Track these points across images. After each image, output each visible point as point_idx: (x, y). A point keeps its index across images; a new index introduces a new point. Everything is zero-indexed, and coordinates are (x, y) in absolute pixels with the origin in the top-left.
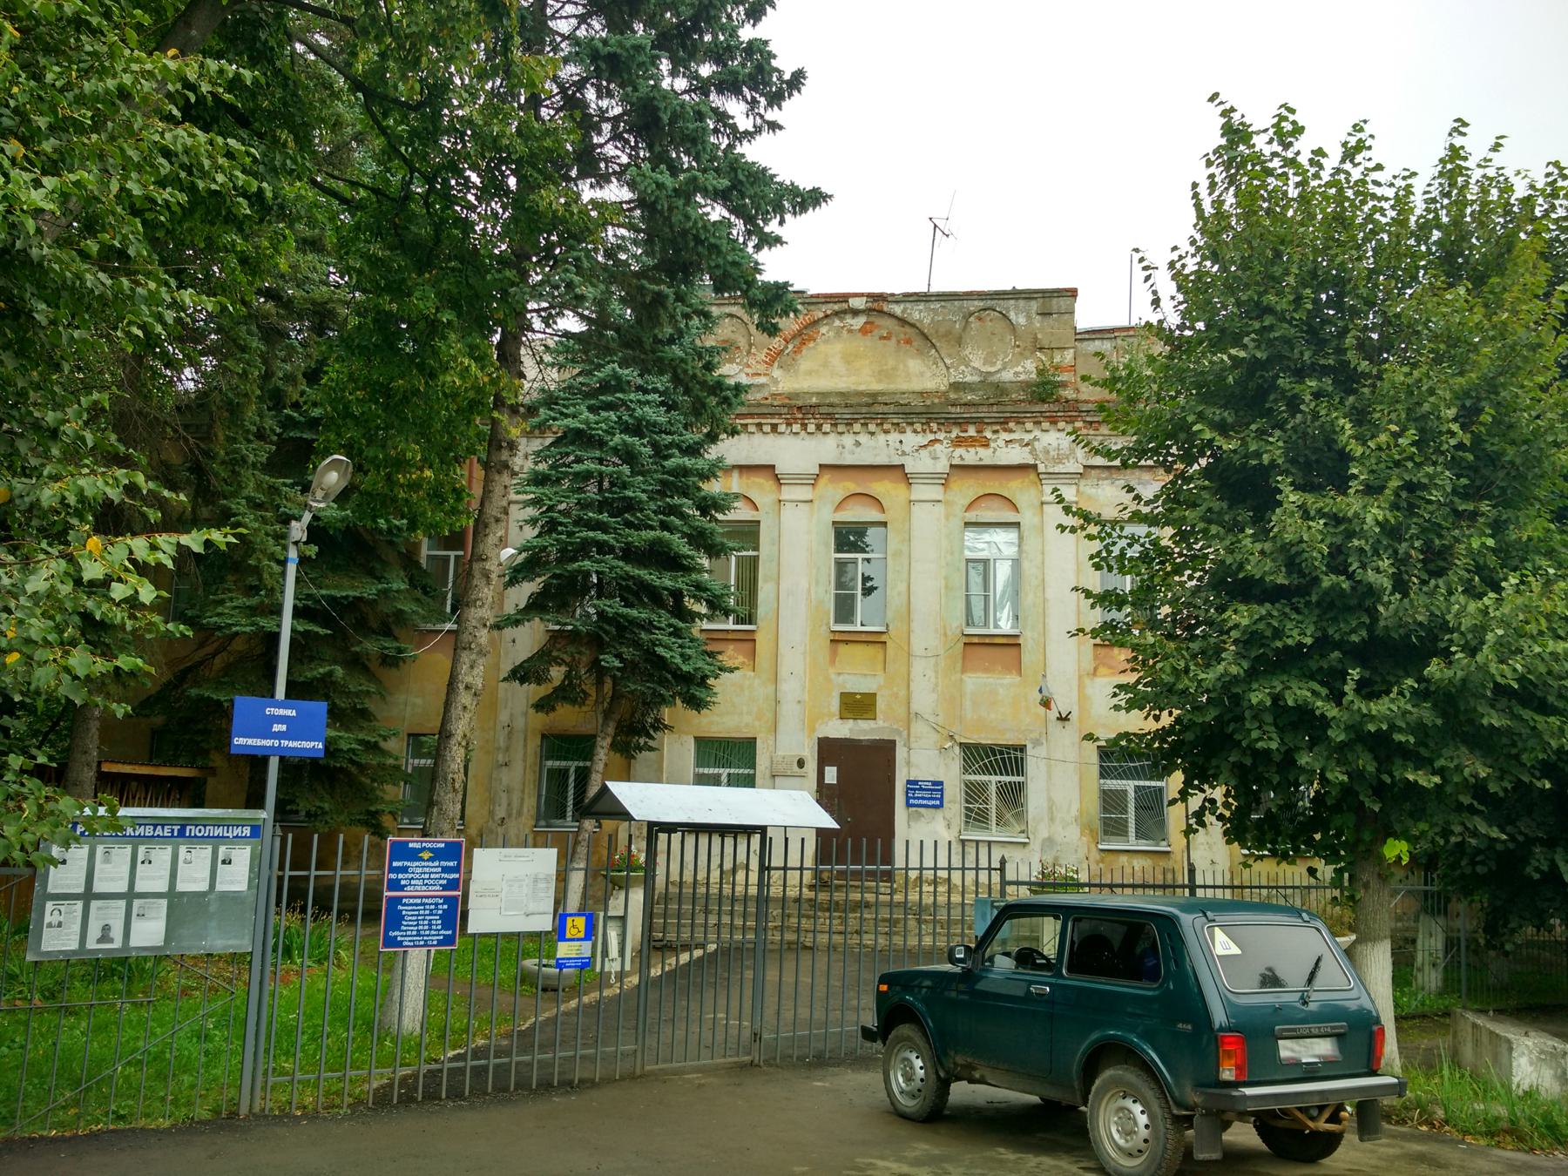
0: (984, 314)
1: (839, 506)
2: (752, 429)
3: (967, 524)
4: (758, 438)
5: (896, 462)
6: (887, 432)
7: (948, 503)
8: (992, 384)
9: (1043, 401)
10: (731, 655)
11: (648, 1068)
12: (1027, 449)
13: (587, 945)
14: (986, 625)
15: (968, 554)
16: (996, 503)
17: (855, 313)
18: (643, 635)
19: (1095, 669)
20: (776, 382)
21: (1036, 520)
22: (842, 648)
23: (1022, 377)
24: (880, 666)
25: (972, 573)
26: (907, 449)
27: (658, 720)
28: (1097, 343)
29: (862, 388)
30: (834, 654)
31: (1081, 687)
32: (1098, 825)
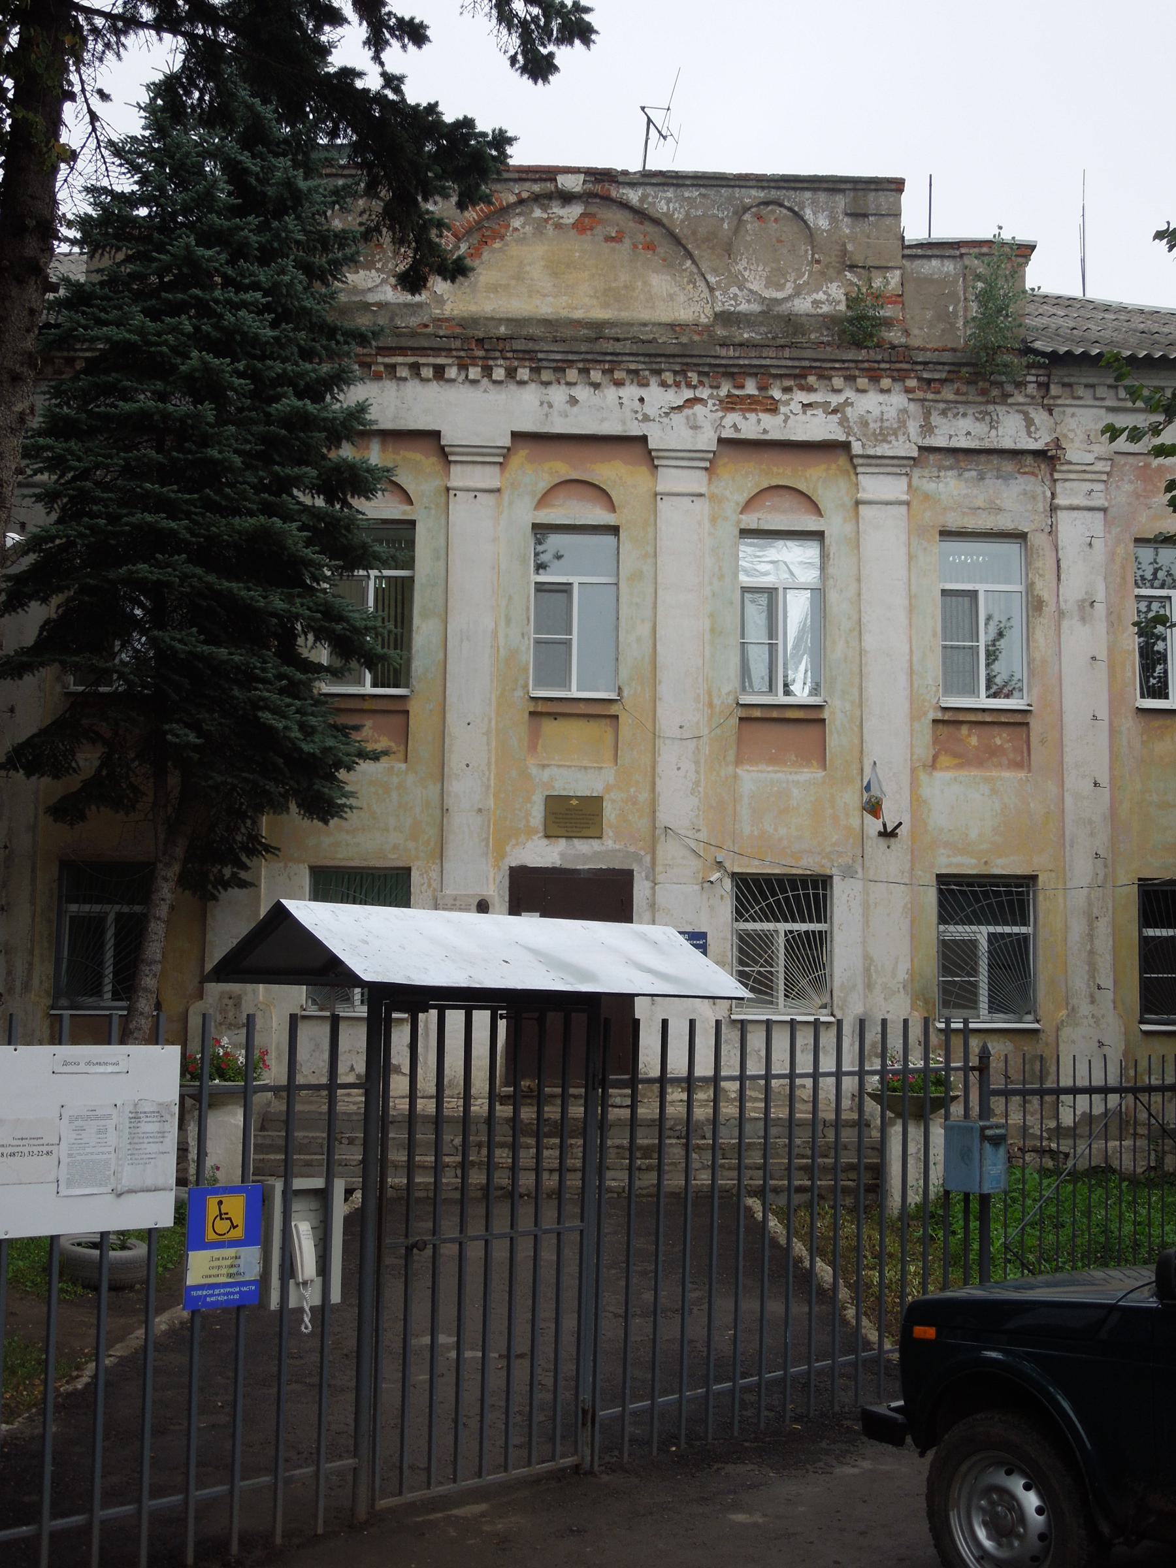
0: (765, 210)
1: (544, 500)
2: (403, 372)
3: (746, 533)
4: (413, 388)
5: (635, 430)
6: (619, 384)
7: (714, 499)
8: (779, 317)
9: (859, 345)
10: (372, 735)
11: (382, 1503)
12: (835, 418)
13: (251, 1256)
14: (771, 688)
15: (745, 580)
16: (787, 501)
17: (567, 198)
18: (236, 692)
19: (935, 758)
20: (440, 300)
21: (849, 528)
22: (549, 727)
23: (825, 309)
24: (609, 754)
25: (751, 609)
26: (651, 410)
27: (254, 838)
28: (935, 263)
29: (578, 315)
30: (535, 736)
31: (914, 784)
32: (935, 993)
